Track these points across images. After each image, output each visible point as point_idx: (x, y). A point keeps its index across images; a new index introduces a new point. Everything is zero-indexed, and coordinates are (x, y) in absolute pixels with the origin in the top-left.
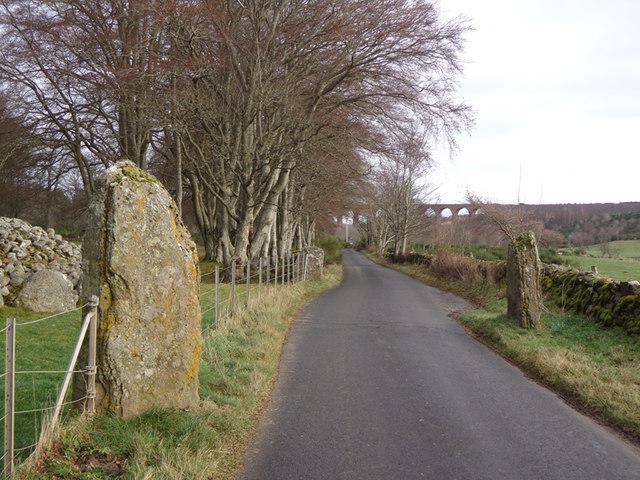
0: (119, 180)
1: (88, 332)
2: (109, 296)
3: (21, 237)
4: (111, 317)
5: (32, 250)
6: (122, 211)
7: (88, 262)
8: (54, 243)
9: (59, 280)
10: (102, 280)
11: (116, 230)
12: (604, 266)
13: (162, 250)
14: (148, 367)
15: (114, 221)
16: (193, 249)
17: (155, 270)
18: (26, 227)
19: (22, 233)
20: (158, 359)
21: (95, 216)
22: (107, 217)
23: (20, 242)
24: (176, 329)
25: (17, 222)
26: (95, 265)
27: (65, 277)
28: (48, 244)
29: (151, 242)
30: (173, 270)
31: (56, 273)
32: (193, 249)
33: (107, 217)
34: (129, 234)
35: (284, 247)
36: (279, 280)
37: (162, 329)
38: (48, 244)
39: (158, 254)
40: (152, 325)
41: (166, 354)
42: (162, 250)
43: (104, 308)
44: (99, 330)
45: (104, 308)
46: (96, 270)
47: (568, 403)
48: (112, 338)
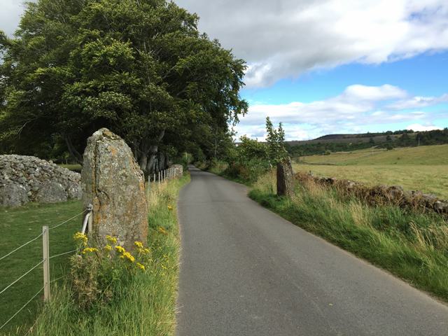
0: (101, 139)
1: (87, 224)
2: (98, 204)
3: (36, 166)
4: (100, 215)
5: (42, 172)
6: (104, 157)
7: (85, 185)
8: (53, 168)
9: (57, 187)
10: (94, 194)
11: (101, 166)
12: (406, 210)
13: (126, 177)
14: (121, 241)
15: (100, 162)
16: (142, 175)
17: (123, 188)
18: (37, 160)
19: (36, 163)
20: (127, 235)
21: (88, 160)
22: (95, 160)
23: (36, 168)
24: (135, 218)
25: (33, 158)
26: (89, 186)
27: (61, 185)
28: (50, 169)
29: (120, 173)
30: (132, 187)
31: (55, 183)
32: (142, 175)
33: (95, 160)
34: (109, 168)
35: (161, 165)
36: (157, 179)
37: (128, 219)
38: (50, 169)
39: (124, 179)
40: (122, 218)
41: (131, 233)
42: (126, 177)
43: (96, 210)
44: (93, 223)
45: (96, 210)
46: (90, 189)
47: (419, 288)
48: (101, 227)
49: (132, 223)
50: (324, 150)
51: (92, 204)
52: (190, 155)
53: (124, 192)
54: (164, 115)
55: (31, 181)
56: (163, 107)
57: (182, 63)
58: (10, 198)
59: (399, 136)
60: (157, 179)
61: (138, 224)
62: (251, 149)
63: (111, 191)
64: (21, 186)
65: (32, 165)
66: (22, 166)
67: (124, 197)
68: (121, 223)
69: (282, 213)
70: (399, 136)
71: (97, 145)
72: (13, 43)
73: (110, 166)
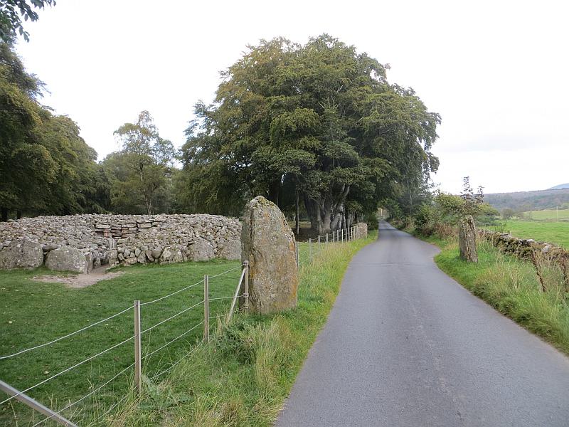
2: (253, 260)
6: (258, 219)
11: (255, 229)
13: (277, 238)
17: (275, 247)
28: (235, 227)
30: (283, 247)
37: (279, 275)
38: (235, 227)
41: (281, 287)
42: (277, 238)
49: (283, 278)
50: (559, 202)
51: (248, 260)
52: (385, 210)
53: (275, 252)
54: (347, 171)
55: (218, 239)
56: (348, 163)
57: (369, 120)
58: (199, 254)
59: (304, 219)
60: (340, 239)
61: (287, 280)
62: (449, 205)
63: (264, 250)
64: (209, 243)
65: (219, 225)
66: (211, 225)
67: (366, 268)
68: (273, 278)
69: (465, 283)
70: (304, 219)
71: (252, 211)
72: (184, 195)
73: (262, 228)
